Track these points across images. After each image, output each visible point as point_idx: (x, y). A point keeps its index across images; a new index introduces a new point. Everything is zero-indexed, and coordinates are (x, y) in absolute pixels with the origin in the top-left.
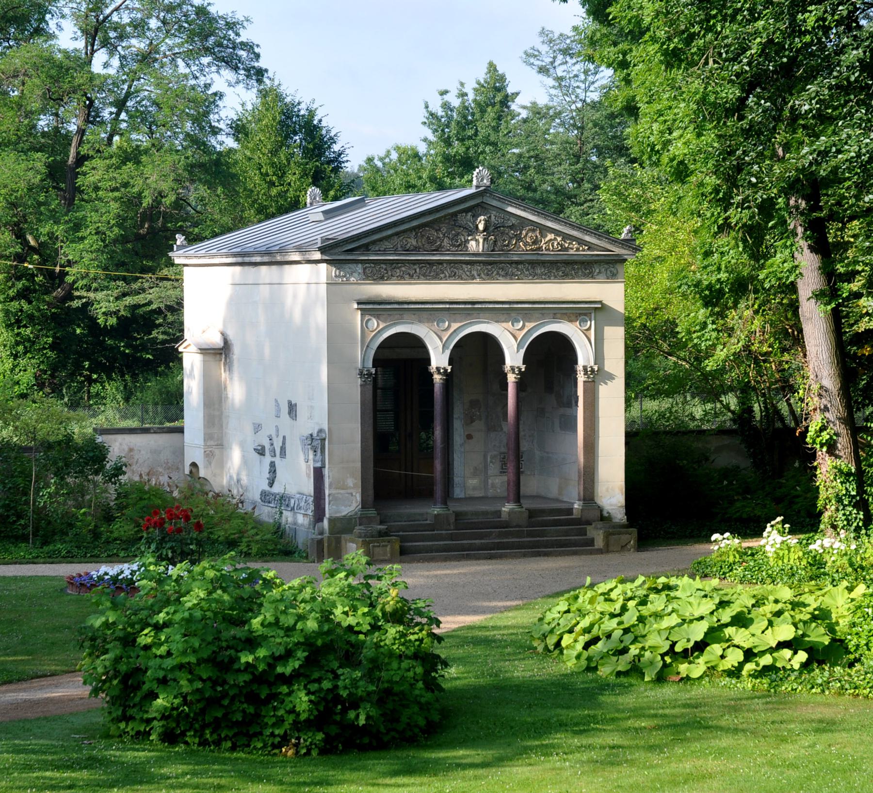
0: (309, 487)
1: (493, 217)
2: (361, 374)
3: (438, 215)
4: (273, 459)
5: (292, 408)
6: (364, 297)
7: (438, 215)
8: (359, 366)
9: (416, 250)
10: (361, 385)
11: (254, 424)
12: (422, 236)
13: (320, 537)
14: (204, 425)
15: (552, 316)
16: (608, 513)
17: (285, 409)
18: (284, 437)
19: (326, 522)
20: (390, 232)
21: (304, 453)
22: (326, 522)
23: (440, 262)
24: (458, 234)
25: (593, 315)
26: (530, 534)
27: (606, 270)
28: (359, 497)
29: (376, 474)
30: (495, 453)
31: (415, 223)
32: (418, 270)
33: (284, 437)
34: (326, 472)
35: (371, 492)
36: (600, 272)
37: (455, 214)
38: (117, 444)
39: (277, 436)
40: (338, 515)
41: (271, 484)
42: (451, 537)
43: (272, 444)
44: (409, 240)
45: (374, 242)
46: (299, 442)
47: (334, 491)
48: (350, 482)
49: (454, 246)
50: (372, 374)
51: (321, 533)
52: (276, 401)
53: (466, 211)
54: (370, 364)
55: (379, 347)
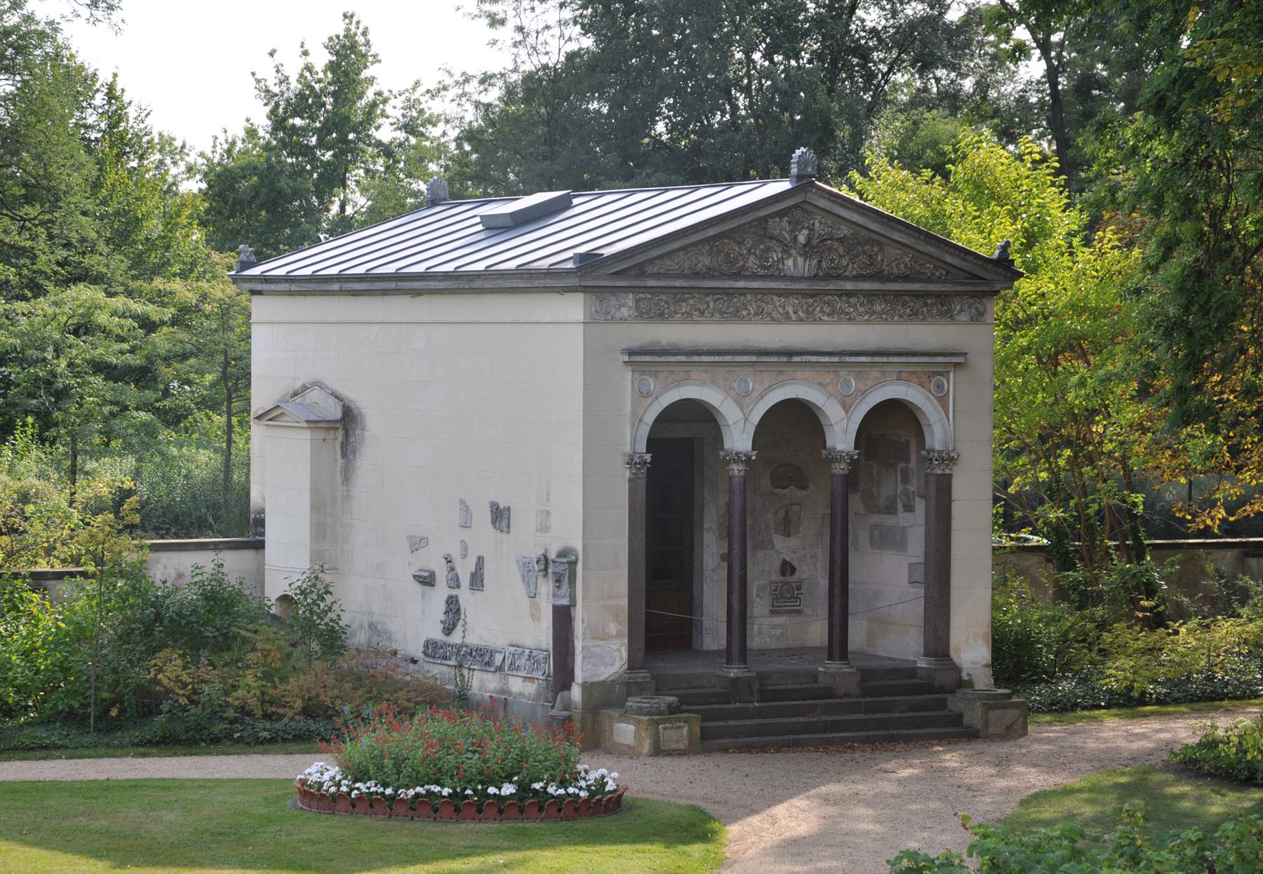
0: (542, 635)
1: (817, 225)
2: (631, 463)
3: (743, 220)
4: (454, 592)
5: (500, 516)
6: (635, 344)
7: (743, 220)
8: (628, 449)
9: (709, 274)
10: (630, 480)
11: (409, 537)
12: (719, 252)
13: (565, 713)
14: (311, 538)
15: (895, 376)
16: (969, 675)
17: (483, 516)
18: (480, 561)
19: (576, 693)
20: (676, 245)
21: (528, 585)
22: (576, 693)
23: (742, 292)
24: (768, 249)
25: (952, 375)
26: (871, 709)
27: (970, 306)
28: (625, 654)
29: (649, 616)
30: (764, 582)
31: (711, 232)
32: (711, 304)
33: (480, 561)
34: (579, 614)
35: (642, 644)
36: (961, 311)
37: (765, 219)
38: (160, 567)
39: (464, 556)
40: (595, 679)
41: (448, 630)
42: (759, 713)
43: (453, 569)
44: (701, 258)
45: (651, 261)
46: (514, 566)
47: (590, 643)
48: (613, 628)
49: (763, 267)
50: (646, 463)
51: (567, 707)
52: (462, 502)
53: (781, 214)
54: (642, 447)
55: (659, 420)
